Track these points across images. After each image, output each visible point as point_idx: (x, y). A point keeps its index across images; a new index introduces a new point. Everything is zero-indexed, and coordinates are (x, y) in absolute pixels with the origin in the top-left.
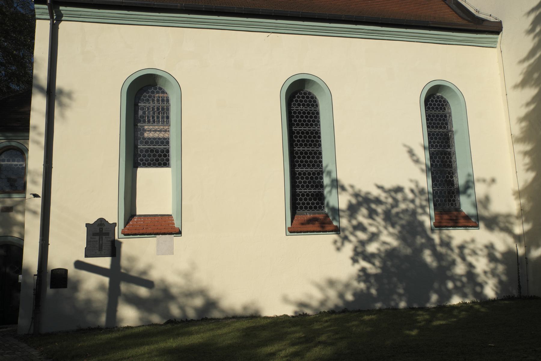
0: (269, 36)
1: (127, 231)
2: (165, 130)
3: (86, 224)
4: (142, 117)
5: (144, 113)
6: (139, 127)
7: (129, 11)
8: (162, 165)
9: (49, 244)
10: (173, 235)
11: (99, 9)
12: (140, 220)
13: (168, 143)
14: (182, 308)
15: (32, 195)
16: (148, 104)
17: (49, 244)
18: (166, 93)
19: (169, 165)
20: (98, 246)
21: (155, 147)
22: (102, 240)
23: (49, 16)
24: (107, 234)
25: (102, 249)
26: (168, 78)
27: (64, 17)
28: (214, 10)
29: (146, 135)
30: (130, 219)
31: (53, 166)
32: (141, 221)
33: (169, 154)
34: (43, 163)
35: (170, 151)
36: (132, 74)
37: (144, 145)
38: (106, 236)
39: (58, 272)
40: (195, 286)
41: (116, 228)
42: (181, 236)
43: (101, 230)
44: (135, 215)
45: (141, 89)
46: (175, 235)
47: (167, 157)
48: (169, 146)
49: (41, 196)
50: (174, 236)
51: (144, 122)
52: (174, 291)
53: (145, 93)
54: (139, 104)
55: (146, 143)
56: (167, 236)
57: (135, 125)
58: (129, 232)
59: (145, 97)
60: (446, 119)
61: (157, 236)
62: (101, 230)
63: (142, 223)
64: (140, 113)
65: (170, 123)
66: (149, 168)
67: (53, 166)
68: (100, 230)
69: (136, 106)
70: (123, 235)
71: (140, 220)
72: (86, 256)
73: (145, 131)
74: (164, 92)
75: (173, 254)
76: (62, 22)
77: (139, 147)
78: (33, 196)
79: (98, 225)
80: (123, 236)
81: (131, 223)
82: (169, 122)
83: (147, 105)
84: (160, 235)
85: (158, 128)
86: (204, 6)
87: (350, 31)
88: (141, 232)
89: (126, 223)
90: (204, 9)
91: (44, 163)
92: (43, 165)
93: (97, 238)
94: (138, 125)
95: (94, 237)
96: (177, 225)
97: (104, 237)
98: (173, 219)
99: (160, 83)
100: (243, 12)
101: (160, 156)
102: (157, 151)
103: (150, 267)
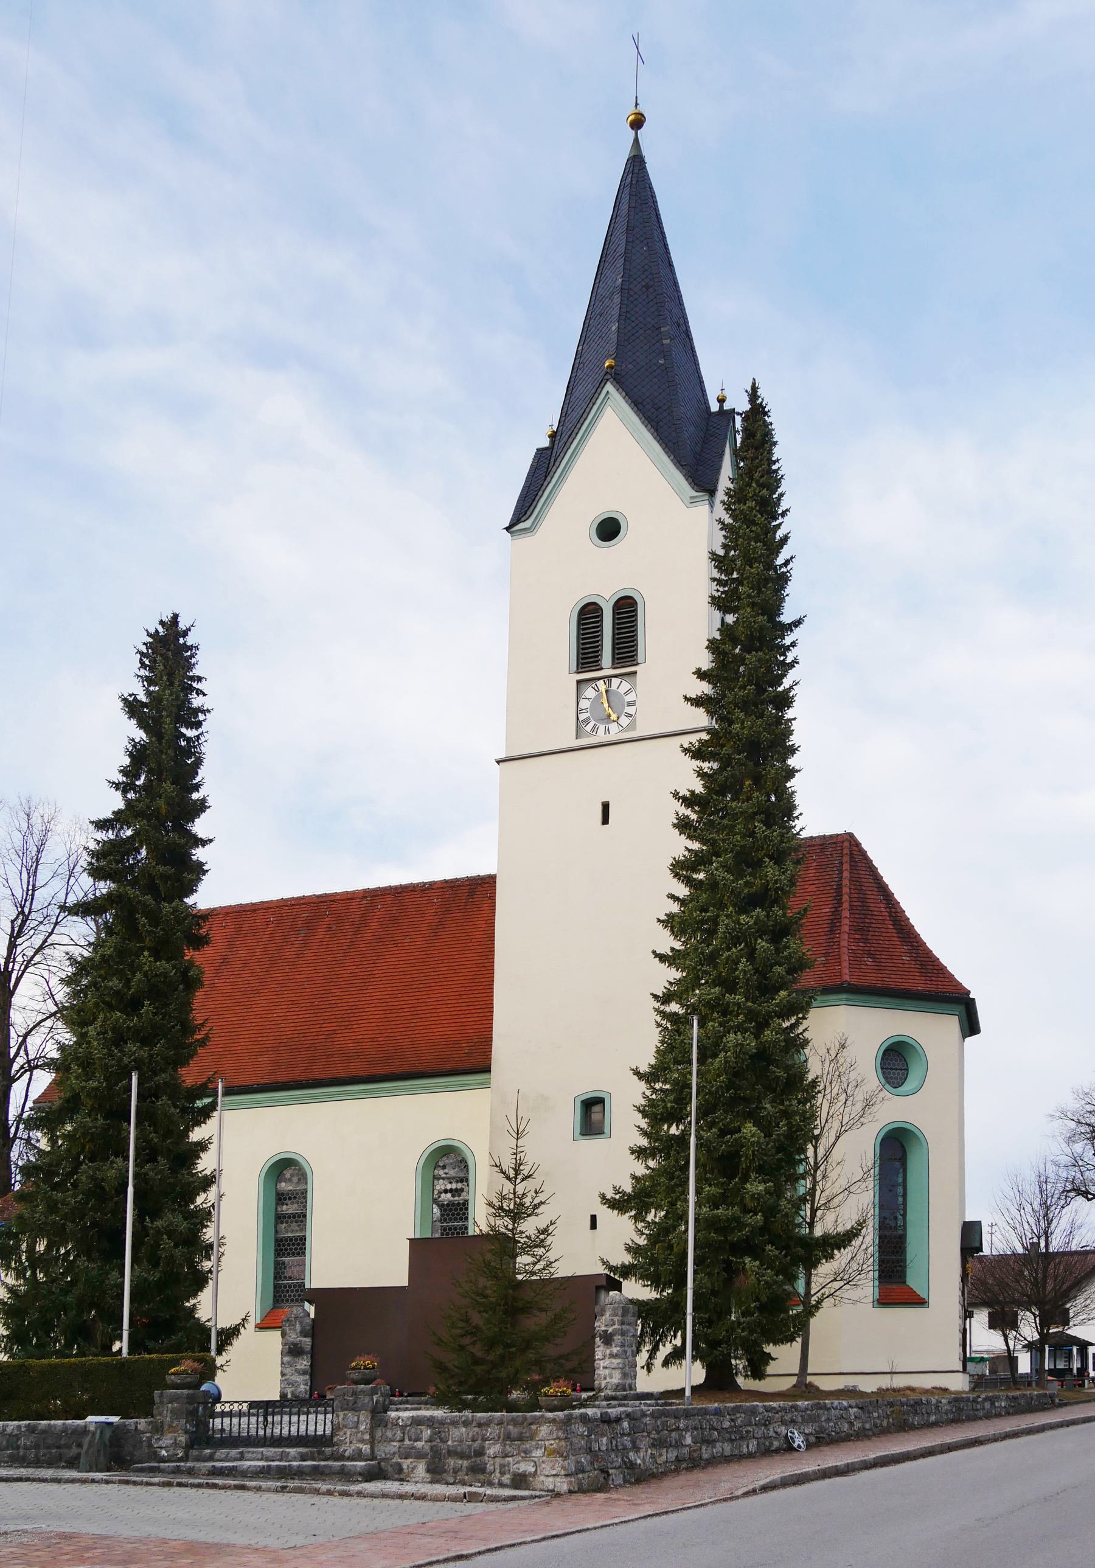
87: (339, 1094)
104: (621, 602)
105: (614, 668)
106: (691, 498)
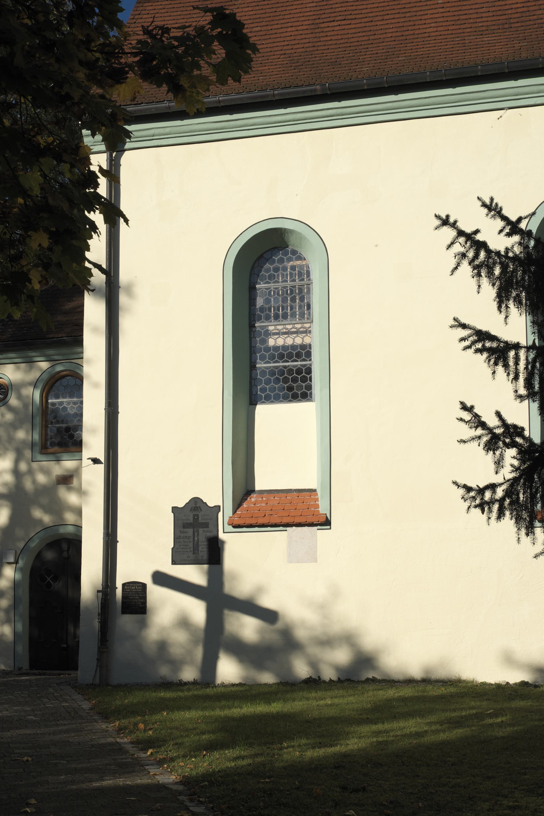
0: (501, 117)
1: (237, 521)
2: (296, 331)
3: (173, 507)
4: (262, 309)
5: (267, 301)
6: (258, 329)
7: (397, 94)
8: (300, 398)
9: (118, 542)
10: (316, 528)
11: (285, 108)
12: (261, 499)
13: (309, 355)
14: (314, 664)
15: (90, 460)
16: (273, 285)
17: (118, 542)
18: (305, 259)
19: (311, 397)
20: (191, 545)
21: (287, 364)
22: (198, 535)
23: (104, 146)
24: (206, 525)
25: (198, 550)
26: (303, 233)
27: (127, 143)
28: (386, 86)
29: (271, 342)
30: (245, 498)
31: (119, 410)
32: (262, 502)
33: (311, 376)
34: (104, 407)
35: (313, 370)
36: (241, 234)
37: (267, 362)
38: (204, 529)
39: (133, 588)
40: (336, 628)
41: (220, 515)
42: (330, 529)
43: (196, 517)
44: (253, 491)
45: (261, 256)
46: (319, 527)
47: (308, 382)
48: (310, 360)
49: (103, 461)
50: (318, 529)
51: (268, 318)
52: (301, 634)
53: (267, 264)
54: (257, 286)
55: (272, 358)
56: (306, 529)
57: (252, 326)
58: (241, 522)
59: (268, 270)
60: (308, 376)
61: (288, 529)
62: (196, 517)
63: (264, 505)
64: (260, 302)
65: (311, 318)
66: (277, 403)
67: (120, 410)
68: (194, 518)
69: (252, 289)
70: (231, 526)
71: (261, 499)
72: (174, 562)
73: (268, 334)
74: (300, 258)
75: (315, 560)
76: (126, 152)
77: (257, 366)
78: (92, 462)
79: (191, 510)
80: (230, 529)
81: (245, 505)
82: (311, 316)
83: (272, 285)
84: (294, 528)
85: (293, 328)
86: (365, 81)
88: (261, 521)
89: (237, 505)
90: (366, 87)
91: (105, 407)
92: (105, 409)
93: (190, 531)
94: (256, 325)
95: (186, 530)
96: (323, 509)
97: (201, 530)
98: (317, 497)
99: (293, 243)
100: (444, 78)
101: (295, 380)
102: (290, 371)
103: (260, 590)
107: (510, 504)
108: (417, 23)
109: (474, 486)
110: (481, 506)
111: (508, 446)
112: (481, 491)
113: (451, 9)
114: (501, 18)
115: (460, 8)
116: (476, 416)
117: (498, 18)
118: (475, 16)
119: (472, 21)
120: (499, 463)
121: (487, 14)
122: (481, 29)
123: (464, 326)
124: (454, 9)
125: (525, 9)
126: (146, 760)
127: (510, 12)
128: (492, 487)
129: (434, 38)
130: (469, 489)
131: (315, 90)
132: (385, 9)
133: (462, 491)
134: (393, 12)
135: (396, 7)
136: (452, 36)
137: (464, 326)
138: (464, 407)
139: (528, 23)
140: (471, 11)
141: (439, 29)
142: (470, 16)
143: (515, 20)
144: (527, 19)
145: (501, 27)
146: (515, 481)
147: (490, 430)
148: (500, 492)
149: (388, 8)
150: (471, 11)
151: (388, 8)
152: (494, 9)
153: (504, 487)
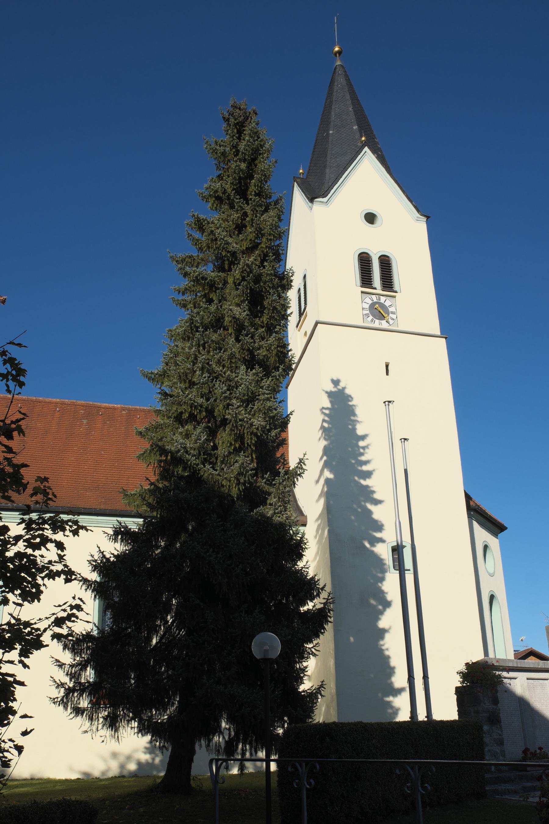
104: (382, 257)
105: (383, 290)
106: (417, 217)
107: (62, 703)
108: (59, 479)
109: (52, 697)
110: (54, 703)
111: (61, 687)
112: (54, 699)
113: (74, 475)
114: (95, 484)
115: (78, 476)
116: (54, 679)
117: (94, 484)
118: (84, 481)
119: (83, 483)
120: (59, 692)
121: (89, 481)
122: (86, 488)
123: (53, 658)
124: (76, 475)
125: (106, 482)
126: (68, 671)
127: (99, 482)
128: (57, 698)
129: (65, 488)
130: (51, 698)
131: (9, 507)
132: (45, 468)
133: (49, 699)
134: (48, 471)
135: (50, 469)
136: (74, 489)
137: (53, 658)
138: (51, 677)
139: (106, 489)
140: (83, 478)
141: (69, 484)
142: (82, 481)
143: (101, 487)
144: (106, 487)
145: (95, 489)
146: (64, 696)
147: (58, 684)
148: (59, 700)
149: (46, 469)
150: (83, 478)
151: (46, 469)
152: (93, 479)
153: (61, 698)
